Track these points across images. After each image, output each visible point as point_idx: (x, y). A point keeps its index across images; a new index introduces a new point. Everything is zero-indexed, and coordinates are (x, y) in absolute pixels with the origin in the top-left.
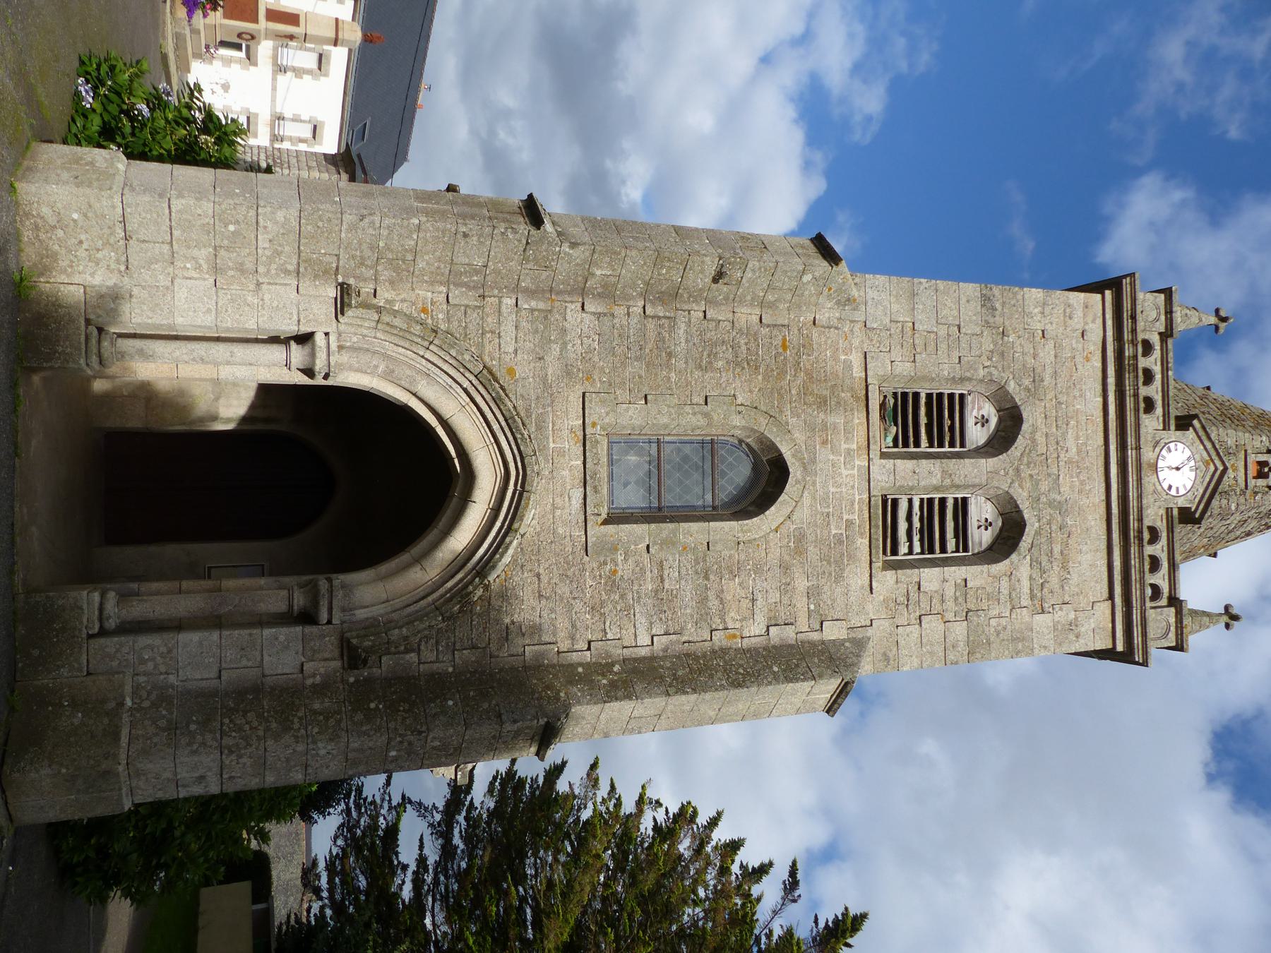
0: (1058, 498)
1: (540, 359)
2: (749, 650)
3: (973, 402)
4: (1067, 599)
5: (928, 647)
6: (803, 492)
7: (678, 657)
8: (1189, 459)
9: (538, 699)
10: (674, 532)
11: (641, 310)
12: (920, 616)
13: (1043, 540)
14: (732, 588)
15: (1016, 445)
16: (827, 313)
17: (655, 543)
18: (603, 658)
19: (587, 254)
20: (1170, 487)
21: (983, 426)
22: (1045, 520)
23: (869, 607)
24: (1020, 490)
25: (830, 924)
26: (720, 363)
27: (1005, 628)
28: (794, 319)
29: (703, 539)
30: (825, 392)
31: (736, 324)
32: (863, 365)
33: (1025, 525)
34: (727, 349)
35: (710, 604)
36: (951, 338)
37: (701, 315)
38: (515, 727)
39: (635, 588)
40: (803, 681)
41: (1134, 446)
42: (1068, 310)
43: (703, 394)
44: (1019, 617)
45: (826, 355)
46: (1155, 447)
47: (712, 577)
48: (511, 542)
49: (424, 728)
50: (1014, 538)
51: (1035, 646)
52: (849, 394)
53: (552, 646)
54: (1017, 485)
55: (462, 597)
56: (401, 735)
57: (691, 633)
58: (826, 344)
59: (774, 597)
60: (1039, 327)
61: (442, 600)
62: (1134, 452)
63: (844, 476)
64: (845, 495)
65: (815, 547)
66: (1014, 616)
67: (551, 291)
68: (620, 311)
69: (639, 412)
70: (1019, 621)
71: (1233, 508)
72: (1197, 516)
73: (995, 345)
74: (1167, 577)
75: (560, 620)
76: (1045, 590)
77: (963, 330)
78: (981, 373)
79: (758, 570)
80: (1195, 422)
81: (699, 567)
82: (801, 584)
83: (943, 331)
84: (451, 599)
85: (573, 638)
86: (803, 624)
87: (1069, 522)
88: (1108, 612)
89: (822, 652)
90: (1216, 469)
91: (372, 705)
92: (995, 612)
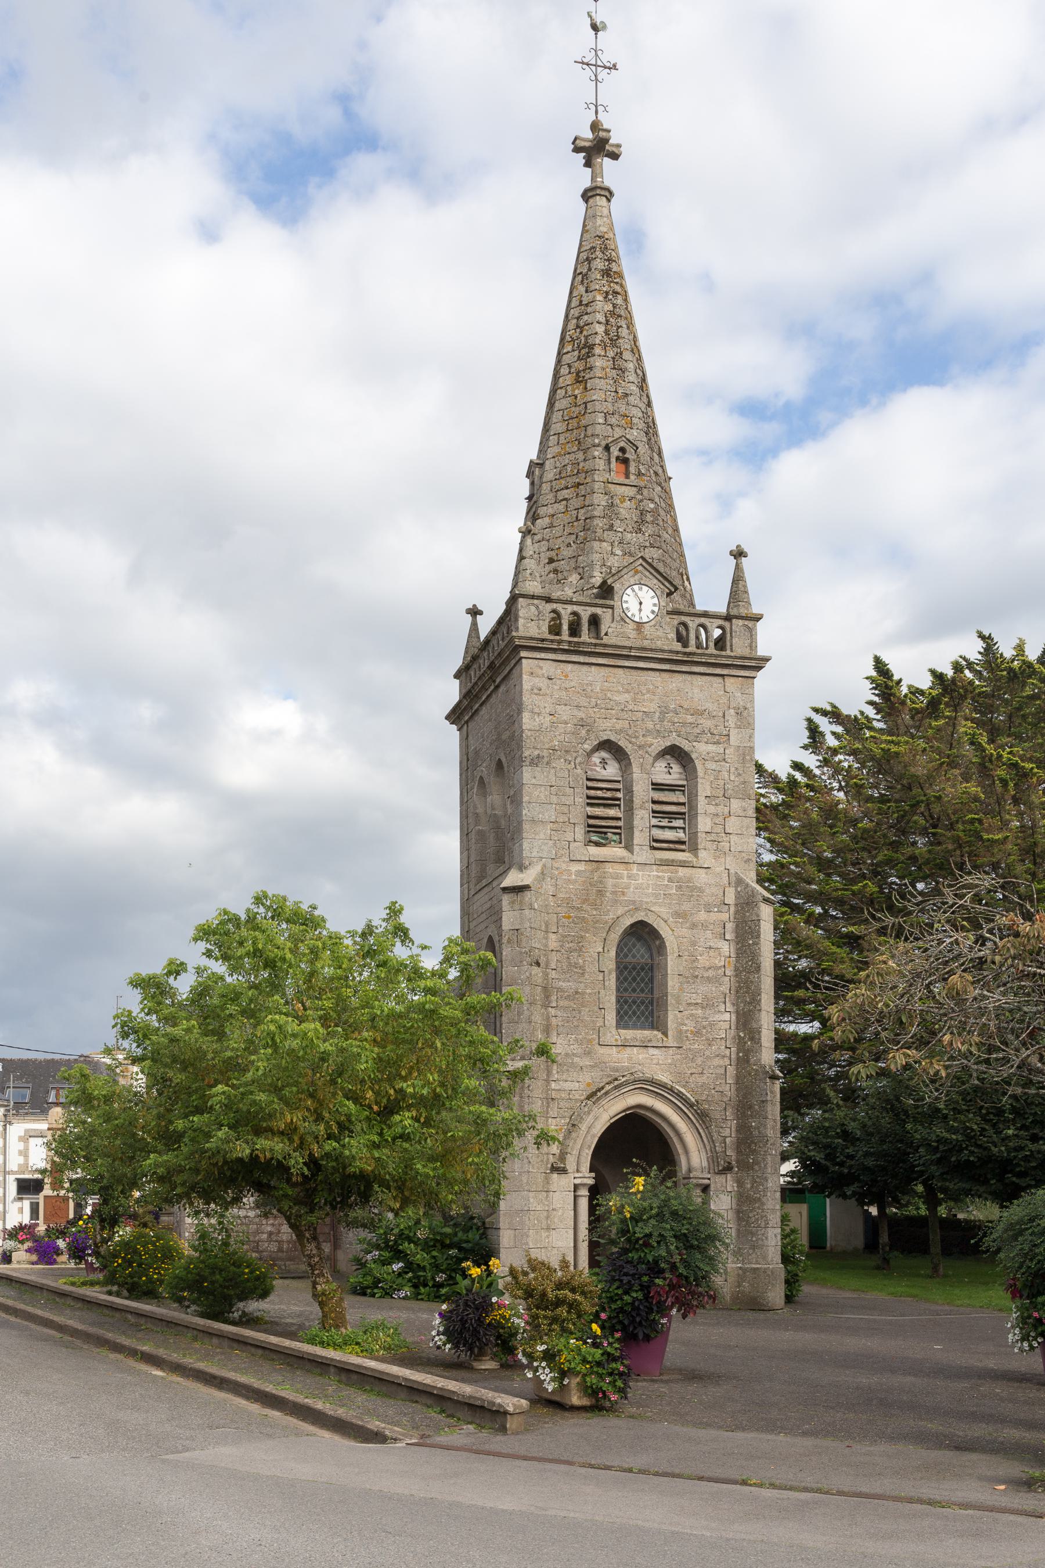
0: (658, 714)
2: (737, 954)
3: (591, 770)
4: (721, 714)
7: (738, 998)
8: (633, 591)
11: (553, 1009)
14: (703, 961)
17: (678, 1007)
25: (877, 692)
26: (580, 961)
35: (711, 975)
37: (554, 972)
42: (536, 691)
43: (598, 973)
46: (625, 622)
47: (697, 973)
57: (725, 988)
58: (565, 888)
60: (549, 718)
66: (729, 761)
68: (554, 1021)
71: (652, 506)
74: (711, 620)
77: (553, 784)
79: (694, 944)
82: (702, 916)
83: (554, 799)
84: (703, 1121)
85: (724, 1057)
86: (725, 916)
88: (732, 680)
89: (743, 908)
90: (641, 565)
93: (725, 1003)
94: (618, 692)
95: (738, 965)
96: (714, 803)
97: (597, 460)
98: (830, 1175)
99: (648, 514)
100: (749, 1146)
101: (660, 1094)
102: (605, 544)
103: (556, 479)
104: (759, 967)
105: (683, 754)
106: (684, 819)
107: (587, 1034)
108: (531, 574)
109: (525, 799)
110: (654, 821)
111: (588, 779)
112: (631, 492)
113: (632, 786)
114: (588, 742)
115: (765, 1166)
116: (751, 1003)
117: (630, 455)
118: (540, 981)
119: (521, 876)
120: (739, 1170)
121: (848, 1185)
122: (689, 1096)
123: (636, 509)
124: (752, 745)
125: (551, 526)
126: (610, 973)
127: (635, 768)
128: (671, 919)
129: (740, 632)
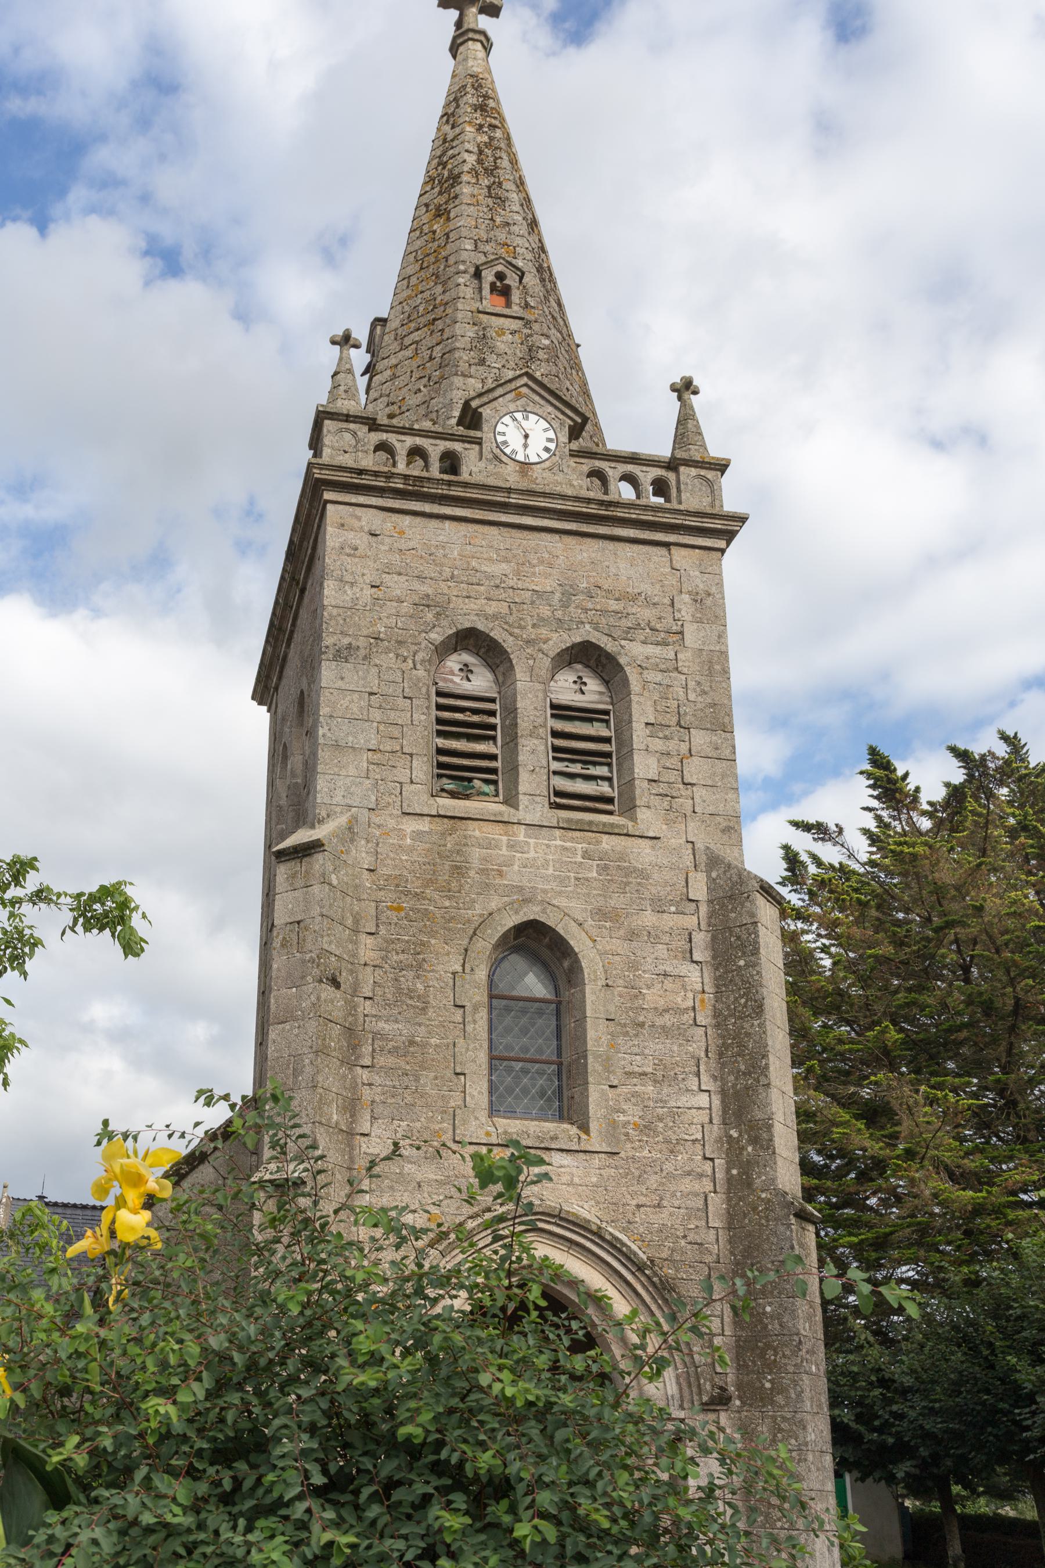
0: (558, 595)
1: (420, 1186)
2: (717, 986)
3: (445, 680)
4: (667, 601)
5: (717, 779)
6: (554, 906)
7: (723, 1065)
8: (515, 419)
9: (768, 1221)
10: (597, 1056)
11: (366, 1071)
12: (684, 784)
13: (604, 621)
14: (653, 997)
15: (500, 641)
16: (361, 854)
17: (608, 1079)
18: (722, 1145)
19: (322, 1130)
20: (547, 449)
21: (471, 672)
22: (582, 616)
23: (674, 842)
24: (551, 642)
25: (875, 793)
26: (420, 986)
27: (699, 683)
28: (369, 894)
29: (603, 1024)
30: (447, 867)
31: (377, 962)
32: (416, 818)
33: (588, 641)
34: (403, 976)
35: (669, 1024)
36: (384, 705)
37: (368, 1003)
38: (796, 1247)
39: (651, 1104)
40: (757, 936)
41: (506, 495)
42: (348, 550)
43: (453, 1009)
44: (687, 664)
45: (407, 861)
46: (501, 461)
47: (641, 1019)
48: (611, 1234)
49: (796, 1338)
50: (600, 656)
51: (718, 648)
52: (449, 839)
53: (709, 1199)
54: (545, 646)
55: (664, 1289)
56: (802, 1362)
57: (697, 1048)
58: (394, 859)
59: (661, 950)
60: (369, 592)
61: (665, 1309)
62: (512, 496)
63: (536, 855)
64: (556, 857)
65: (611, 898)
66: (685, 670)
67: (350, 1169)
68: (366, 1093)
69: (474, 1083)
70: (691, 664)
71: (547, 342)
72: (580, 421)
73: (390, 651)
74: (644, 468)
75: (683, 1188)
76: (658, 626)
77: (375, 690)
78: (421, 673)
79: (634, 966)
80: (474, 404)
81: (632, 1032)
82: (649, 919)
83: (376, 715)
84: (666, 1301)
85: (701, 1176)
86: (691, 922)
87: (584, 585)
88: (684, 552)
89: (723, 906)
90: (526, 385)
91: (768, 1385)
92: (681, 692)
93: (698, 1074)
94: (490, 560)
95: (719, 1006)
96: (661, 735)
97: (462, 287)
98: (864, 1447)
99: (540, 351)
100: (762, 1356)
101: (578, 1244)
102: (472, 381)
103: (403, 325)
104: (761, 1006)
105: (603, 660)
106: (609, 765)
107: (430, 1119)
108: (346, 391)
109: (324, 711)
110: (556, 766)
111: (439, 694)
112: (516, 325)
113: (515, 701)
114: (437, 629)
115: (799, 1395)
116: (750, 1074)
117: (512, 280)
118: (338, 1014)
119: (312, 832)
120: (743, 1403)
121: (894, 1463)
122: (634, 1247)
123: (522, 344)
124: (723, 648)
125: (394, 377)
126: (476, 1009)
127: (521, 674)
128: (590, 922)
129: (694, 486)
